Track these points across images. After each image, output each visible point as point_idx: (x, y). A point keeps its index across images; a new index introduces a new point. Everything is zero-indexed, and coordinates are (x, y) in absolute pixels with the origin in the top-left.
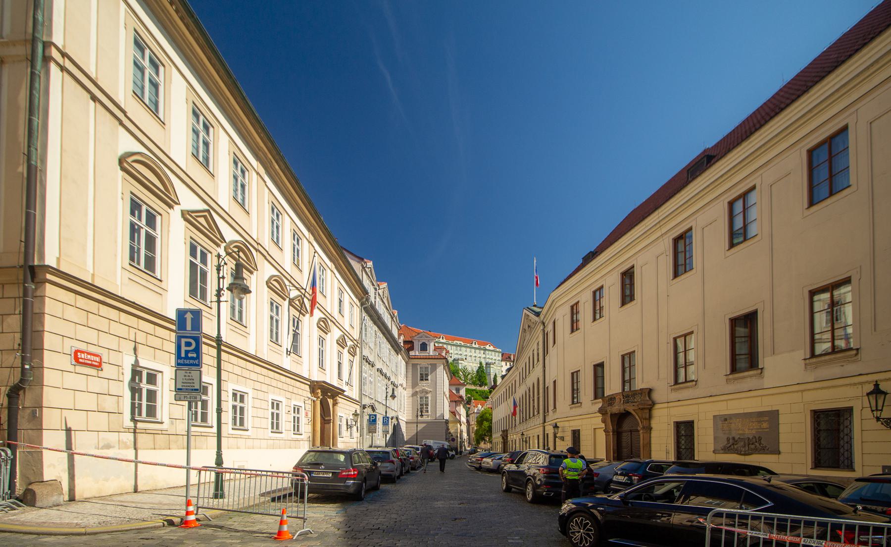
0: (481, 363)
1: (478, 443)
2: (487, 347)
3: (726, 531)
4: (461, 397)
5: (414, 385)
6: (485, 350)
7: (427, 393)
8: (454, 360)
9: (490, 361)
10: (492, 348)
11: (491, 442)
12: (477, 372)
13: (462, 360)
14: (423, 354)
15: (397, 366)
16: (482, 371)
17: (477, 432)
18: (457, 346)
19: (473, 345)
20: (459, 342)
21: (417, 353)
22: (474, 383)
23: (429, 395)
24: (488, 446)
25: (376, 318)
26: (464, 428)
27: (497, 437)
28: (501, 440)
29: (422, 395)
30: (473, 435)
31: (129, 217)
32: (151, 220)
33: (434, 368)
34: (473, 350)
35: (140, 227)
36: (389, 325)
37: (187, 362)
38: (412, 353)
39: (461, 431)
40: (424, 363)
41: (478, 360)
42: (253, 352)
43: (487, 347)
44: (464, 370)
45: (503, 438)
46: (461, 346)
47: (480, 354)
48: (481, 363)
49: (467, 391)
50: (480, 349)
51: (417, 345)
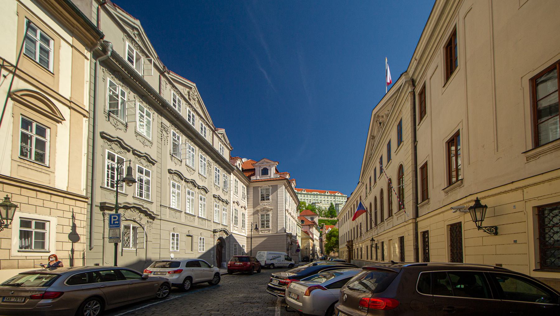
0: (331, 204)
1: (328, 252)
2: (337, 194)
3: (35, 232)
4: (314, 222)
5: (255, 205)
6: (336, 196)
7: (268, 211)
8: (313, 203)
9: (339, 202)
10: (340, 194)
11: (338, 251)
12: (329, 209)
13: (318, 203)
14: (265, 178)
15: (237, 189)
16: (333, 208)
17: (326, 245)
18: (314, 195)
19: (326, 194)
20: (315, 193)
21: (258, 178)
22: (327, 216)
23: (270, 213)
24: (337, 254)
25: (159, 105)
26: (317, 243)
27: (343, 247)
28: (346, 249)
29: (263, 213)
30: (324, 249)
31: (20, 130)
32: (41, 131)
33: (275, 188)
34: (326, 197)
35: (31, 137)
36: (155, 86)
37: (114, 226)
38: (253, 178)
39: (314, 246)
40: (265, 185)
41: (330, 202)
42: (8, 175)
43: (337, 194)
44: (319, 209)
45: (348, 247)
46: (317, 195)
47: (331, 199)
48: (331, 204)
49: (319, 220)
50: (331, 196)
51: (258, 171)
